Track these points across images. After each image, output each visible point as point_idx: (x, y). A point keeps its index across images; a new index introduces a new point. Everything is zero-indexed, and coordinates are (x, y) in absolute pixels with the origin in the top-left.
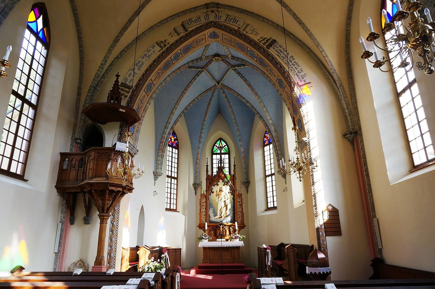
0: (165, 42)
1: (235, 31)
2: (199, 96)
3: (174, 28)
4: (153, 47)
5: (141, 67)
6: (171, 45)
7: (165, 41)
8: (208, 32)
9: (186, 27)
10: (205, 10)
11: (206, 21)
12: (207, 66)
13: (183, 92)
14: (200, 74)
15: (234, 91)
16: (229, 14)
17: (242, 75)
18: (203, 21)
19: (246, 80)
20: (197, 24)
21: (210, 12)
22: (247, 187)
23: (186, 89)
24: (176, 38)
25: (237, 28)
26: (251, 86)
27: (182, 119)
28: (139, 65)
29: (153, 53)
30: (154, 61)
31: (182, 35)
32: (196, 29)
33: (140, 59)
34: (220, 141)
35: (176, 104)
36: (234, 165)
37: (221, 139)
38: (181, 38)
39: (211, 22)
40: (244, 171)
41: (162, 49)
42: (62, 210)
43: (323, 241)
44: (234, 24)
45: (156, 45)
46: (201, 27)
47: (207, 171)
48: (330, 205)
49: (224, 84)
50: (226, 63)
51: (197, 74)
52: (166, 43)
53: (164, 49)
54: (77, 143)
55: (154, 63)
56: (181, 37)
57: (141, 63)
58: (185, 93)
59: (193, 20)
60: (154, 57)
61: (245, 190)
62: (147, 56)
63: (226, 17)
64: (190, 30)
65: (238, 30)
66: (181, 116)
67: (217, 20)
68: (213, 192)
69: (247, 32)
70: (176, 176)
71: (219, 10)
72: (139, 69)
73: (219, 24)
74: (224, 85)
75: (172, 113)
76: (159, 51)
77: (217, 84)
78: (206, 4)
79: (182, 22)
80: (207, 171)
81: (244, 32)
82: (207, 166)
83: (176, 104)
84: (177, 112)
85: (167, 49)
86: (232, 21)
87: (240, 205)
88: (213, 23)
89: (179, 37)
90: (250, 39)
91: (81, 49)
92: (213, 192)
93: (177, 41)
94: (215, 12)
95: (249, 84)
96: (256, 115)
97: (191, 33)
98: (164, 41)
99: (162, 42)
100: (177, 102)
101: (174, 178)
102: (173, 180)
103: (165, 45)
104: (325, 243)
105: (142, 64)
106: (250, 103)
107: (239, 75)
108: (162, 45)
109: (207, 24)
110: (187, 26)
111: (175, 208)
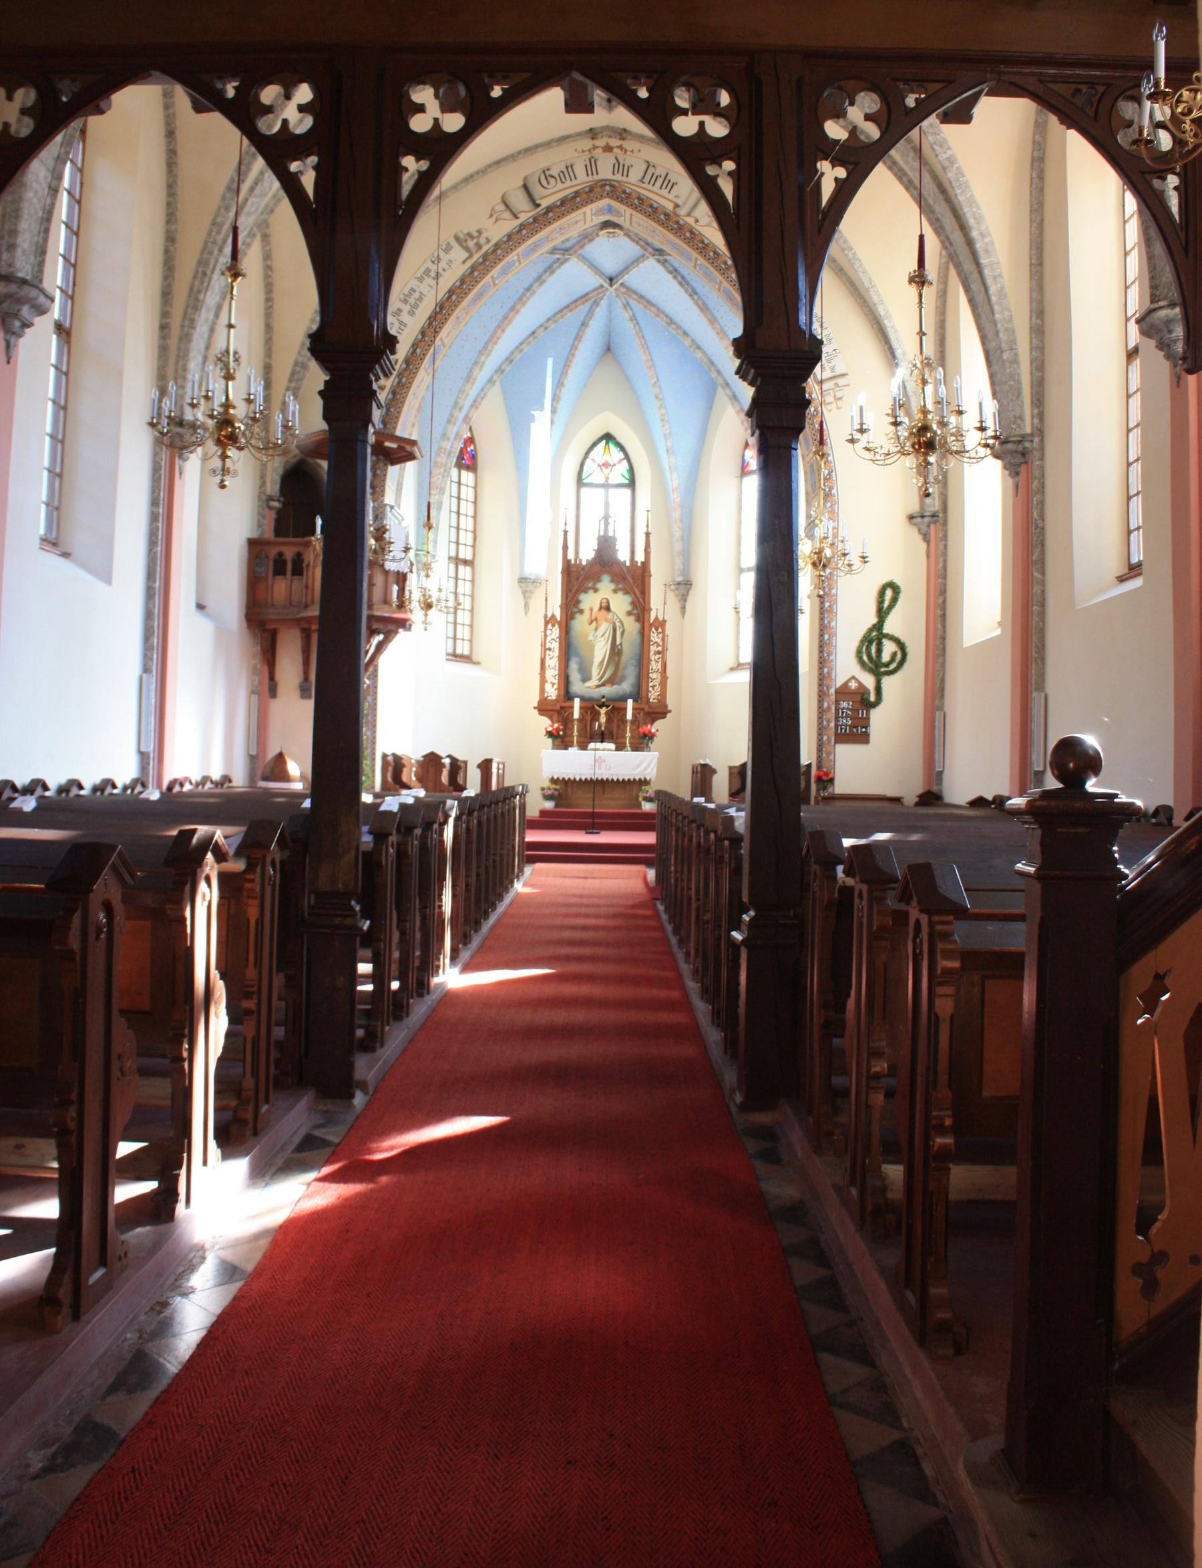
0: (478, 237)
1: (666, 215)
2: (549, 319)
3: (503, 197)
4: (448, 248)
5: (416, 306)
6: (496, 245)
7: (480, 232)
8: (590, 215)
9: (536, 196)
10: (587, 144)
11: (590, 178)
12: (582, 247)
13: (505, 318)
14: (559, 267)
15: (658, 309)
16: (653, 160)
17: (683, 278)
18: (582, 179)
19: (696, 293)
20: (563, 186)
21: (599, 151)
22: (684, 599)
23: (514, 309)
24: (510, 225)
25: (669, 206)
26: (708, 309)
27: (495, 394)
28: (412, 301)
29: (446, 267)
30: (451, 292)
31: (523, 217)
32: (563, 202)
33: (414, 283)
34: (607, 443)
35: (481, 353)
36: (648, 535)
37: (608, 437)
38: (522, 226)
39: (603, 183)
40: (678, 547)
41: (470, 256)
42: (255, 668)
43: (828, 754)
44: (664, 192)
45: (453, 243)
46: (575, 197)
47: (565, 548)
48: (853, 678)
49: (628, 284)
50: (637, 243)
51: (550, 267)
52: (482, 241)
53: (476, 257)
54: (270, 508)
55: (450, 297)
56: (521, 225)
57: (416, 295)
58: (510, 322)
59: (554, 172)
60: (450, 279)
61: (677, 605)
62: (433, 274)
63: (644, 168)
64: (545, 203)
65: (675, 213)
66: (494, 383)
67: (618, 177)
68: (581, 612)
69: (697, 221)
70: (469, 557)
71: (626, 144)
72: (411, 313)
73: (624, 192)
74: (628, 289)
75: (469, 378)
76: (464, 262)
77: (606, 285)
78: (591, 130)
79: (525, 179)
80: (565, 548)
81: (690, 221)
82: (566, 532)
83: (481, 353)
84: (482, 376)
85: (485, 257)
86: (660, 181)
87: (659, 653)
88: (608, 188)
89: (518, 222)
90: (702, 242)
91: (269, 263)
92: (581, 612)
93: (509, 236)
94: (616, 150)
95: (704, 304)
96: (720, 389)
97: (547, 213)
98: (476, 234)
99: (470, 235)
100: (485, 348)
101: (465, 562)
102: (461, 567)
103: (479, 246)
104: (832, 757)
105: (420, 299)
106: (704, 352)
107: (675, 277)
108: (471, 244)
109: (591, 189)
110: (537, 191)
111: (466, 652)
